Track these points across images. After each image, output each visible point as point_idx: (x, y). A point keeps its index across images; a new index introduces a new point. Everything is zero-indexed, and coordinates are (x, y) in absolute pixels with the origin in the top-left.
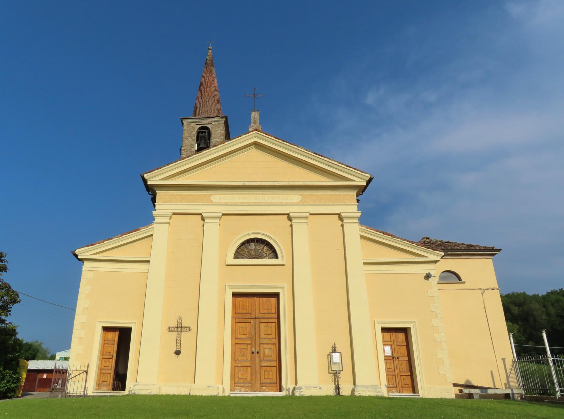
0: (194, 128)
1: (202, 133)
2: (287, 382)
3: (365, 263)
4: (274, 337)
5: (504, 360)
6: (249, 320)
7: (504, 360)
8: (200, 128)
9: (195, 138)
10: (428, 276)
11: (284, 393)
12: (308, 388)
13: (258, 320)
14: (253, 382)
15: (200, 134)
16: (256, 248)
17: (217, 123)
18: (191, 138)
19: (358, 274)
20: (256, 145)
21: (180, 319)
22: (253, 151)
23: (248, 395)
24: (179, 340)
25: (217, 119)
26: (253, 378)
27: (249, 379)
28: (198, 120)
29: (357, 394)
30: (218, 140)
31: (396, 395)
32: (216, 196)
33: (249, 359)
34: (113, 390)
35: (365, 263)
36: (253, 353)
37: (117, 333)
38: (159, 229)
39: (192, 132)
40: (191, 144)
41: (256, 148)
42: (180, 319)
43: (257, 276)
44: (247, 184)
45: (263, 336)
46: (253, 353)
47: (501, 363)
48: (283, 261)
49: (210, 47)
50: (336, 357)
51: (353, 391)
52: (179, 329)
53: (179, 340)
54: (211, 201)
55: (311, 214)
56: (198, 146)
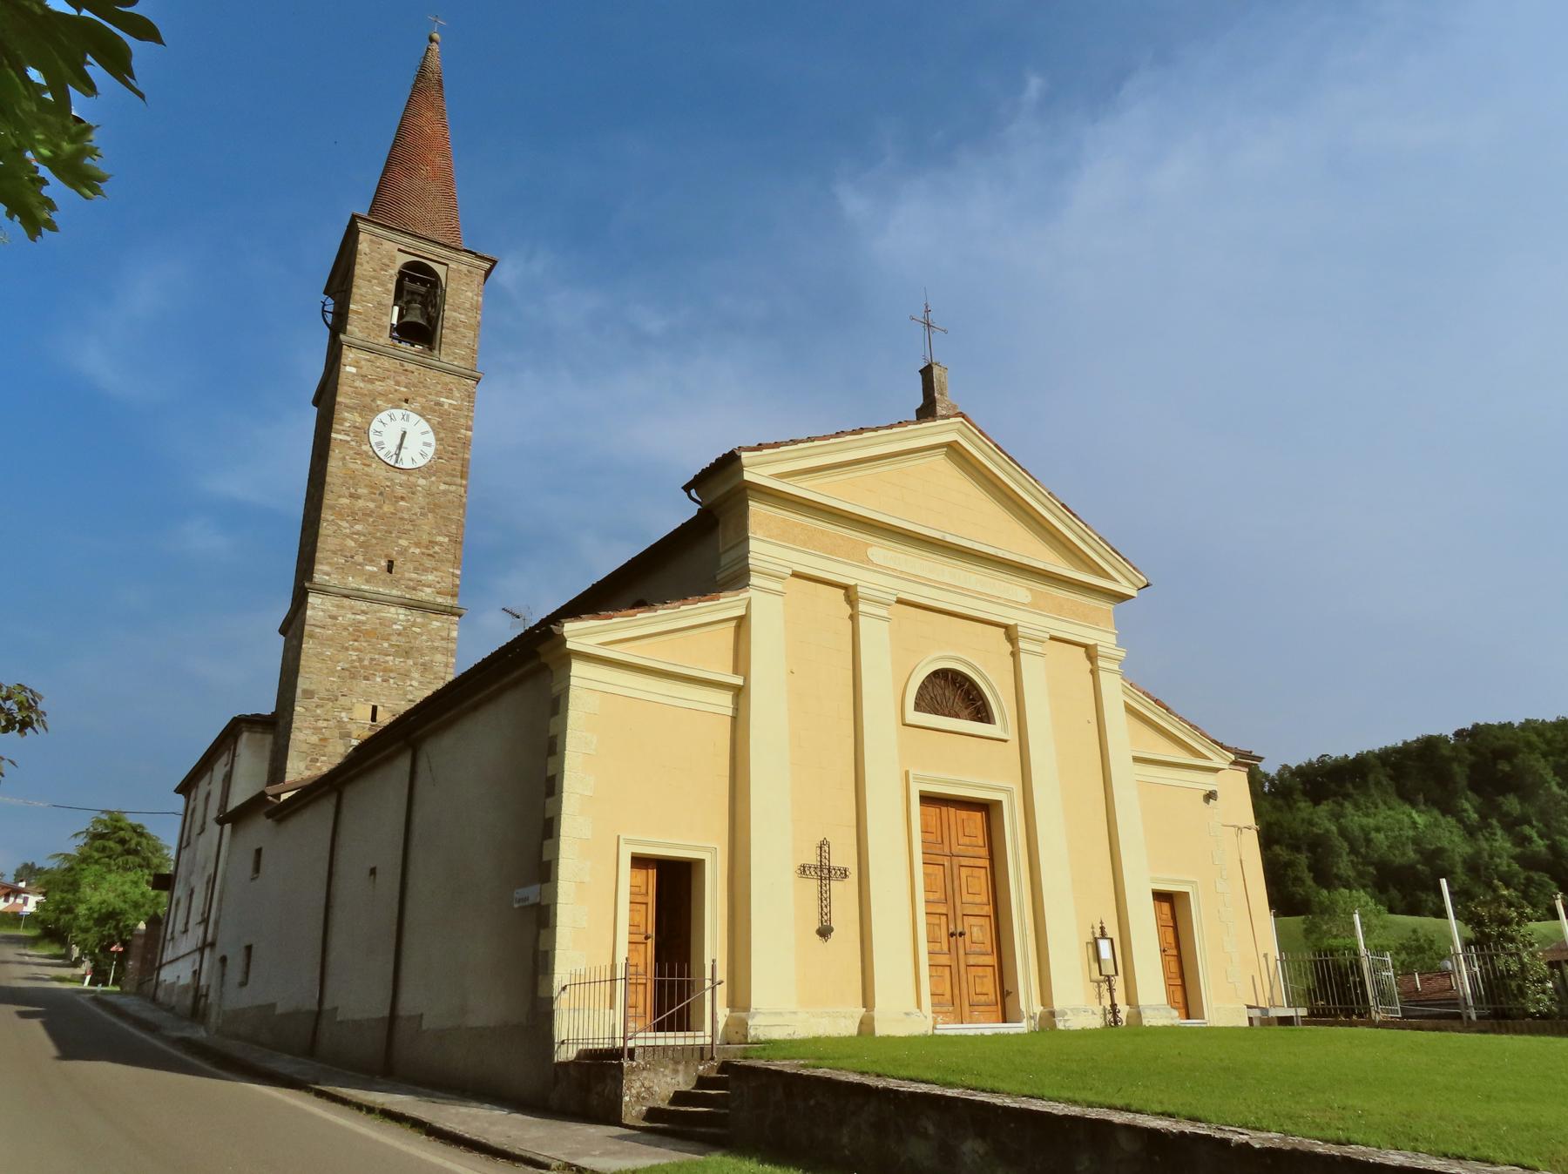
0: (393, 259)
1: (413, 280)
2: (1028, 999)
3: (1136, 759)
4: (985, 900)
5: (1265, 956)
6: (940, 860)
7: (1265, 956)
8: (408, 266)
9: (392, 287)
10: (1210, 796)
11: (1023, 1027)
12: (1075, 1011)
13: (955, 860)
14: (957, 1001)
15: (407, 282)
16: (954, 693)
17: (464, 268)
18: (382, 284)
19: (1124, 773)
20: (953, 450)
21: (823, 846)
22: (940, 461)
23: (964, 1032)
24: (824, 900)
25: (465, 258)
26: (956, 992)
27: (948, 996)
28: (408, 240)
29: (881, 1030)
30: (463, 317)
31: (952, 1029)
32: (882, 552)
33: (945, 948)
34: (659, 1027)
35: (1136, 759)
36: (952, 935)
37: (652, 873)
38: (765, 603)
39: (385, 267)
40: (380, 303)
41: (947, 454)
42: (823, 846)
43: (965, 760)
44: (949, 539)
45: (966, 898)
46: (952, 935)
47: (1263, 960)
48: (1005, 729)
49: (436, 36)
50: (1104, 946)
51: (866, 1025)
52: (823, 872)
53: (824, 900)
54: (869, 561)
55: (1053, 638)
56: (401, 316)
